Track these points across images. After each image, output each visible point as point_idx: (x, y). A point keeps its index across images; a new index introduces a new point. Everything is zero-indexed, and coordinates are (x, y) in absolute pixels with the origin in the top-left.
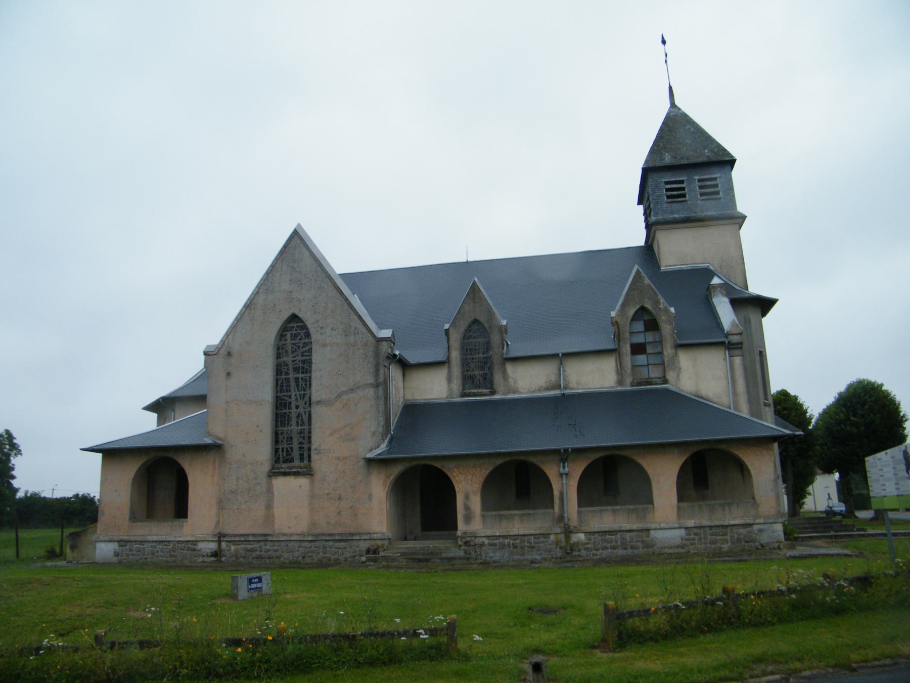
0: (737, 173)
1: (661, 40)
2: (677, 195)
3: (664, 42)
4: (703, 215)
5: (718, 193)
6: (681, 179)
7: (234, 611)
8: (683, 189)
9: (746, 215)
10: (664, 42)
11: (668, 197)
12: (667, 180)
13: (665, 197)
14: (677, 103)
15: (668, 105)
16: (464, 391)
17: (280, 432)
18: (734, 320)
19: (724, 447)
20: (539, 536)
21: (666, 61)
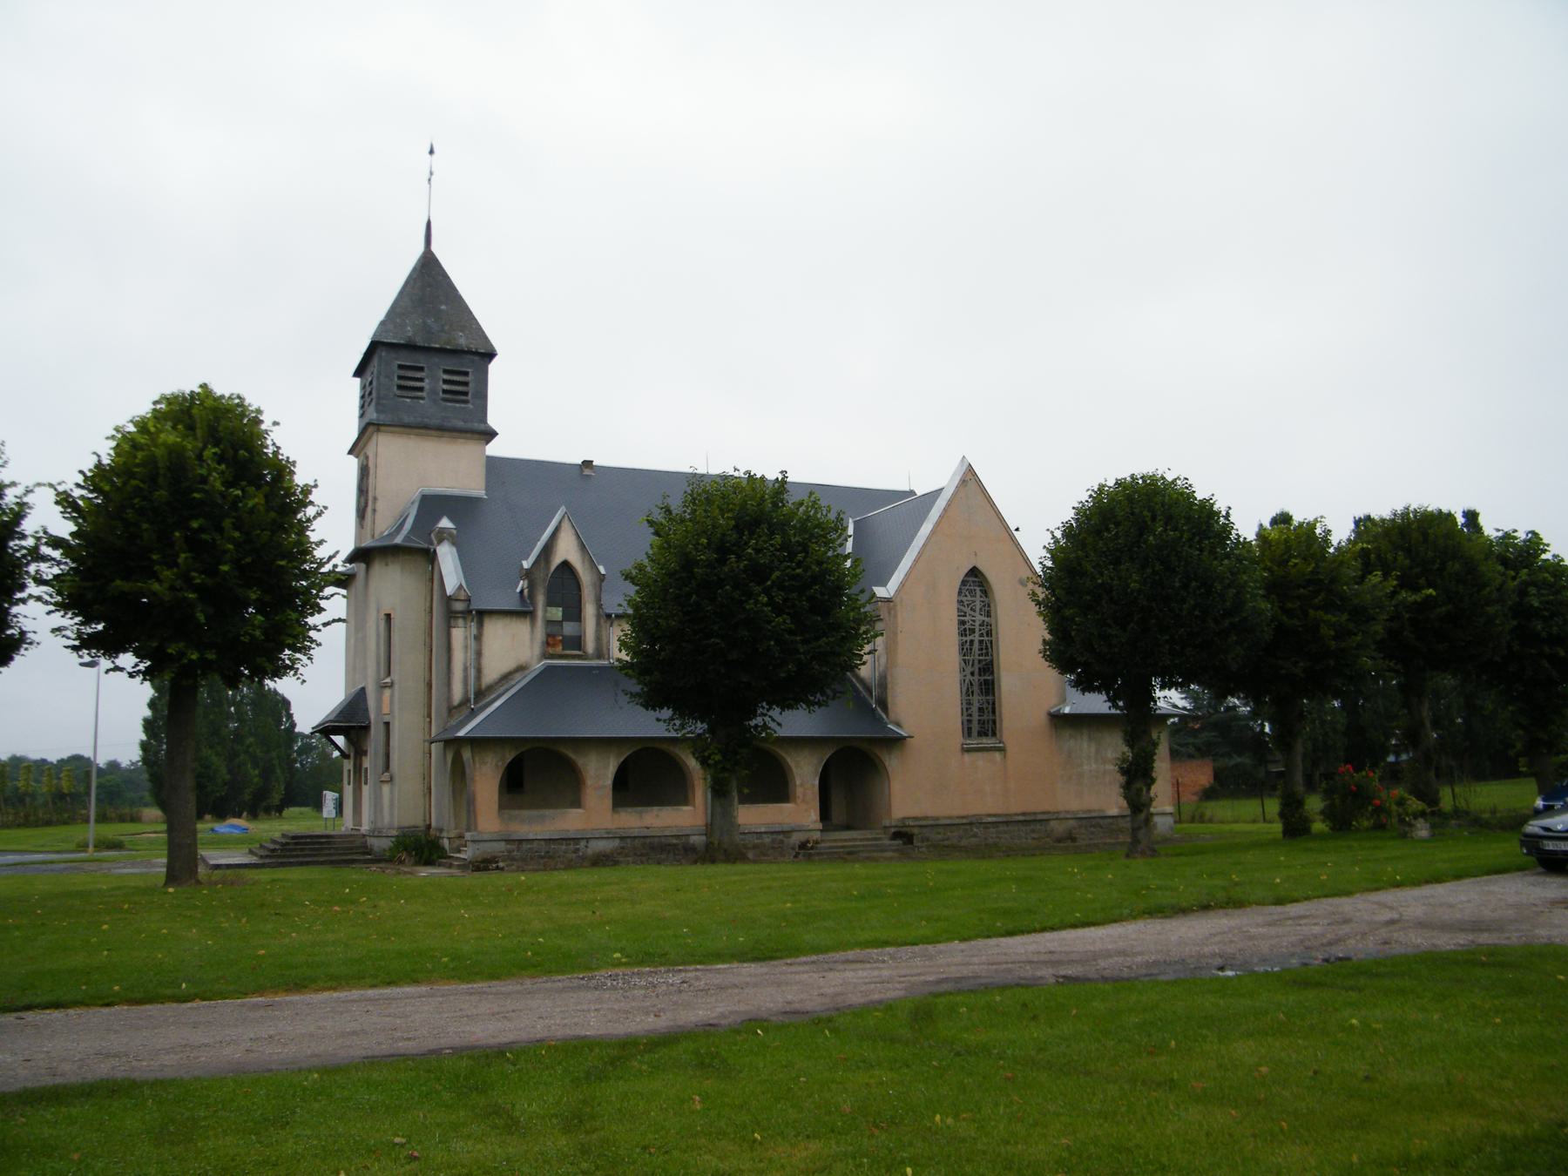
0: (494, 368)
1: (429, 150)
2: (408, 387)
3: (431, 152)
4: (449, 424)
5: (421, 389)
6: (421, 365)
7: (776, 1044)
8: (466, 384)
9: (497, 430)
10: (431, 152)
11: (400, 387)
12: (403, 363)
13: (395, 387)
14: (434, 248)
15: (421, 249)
16: (1351, 626)
17: (991, 714)
18: (461, 585)
19: (664, 746)
20: (989, 825)
21: (429, 180)
